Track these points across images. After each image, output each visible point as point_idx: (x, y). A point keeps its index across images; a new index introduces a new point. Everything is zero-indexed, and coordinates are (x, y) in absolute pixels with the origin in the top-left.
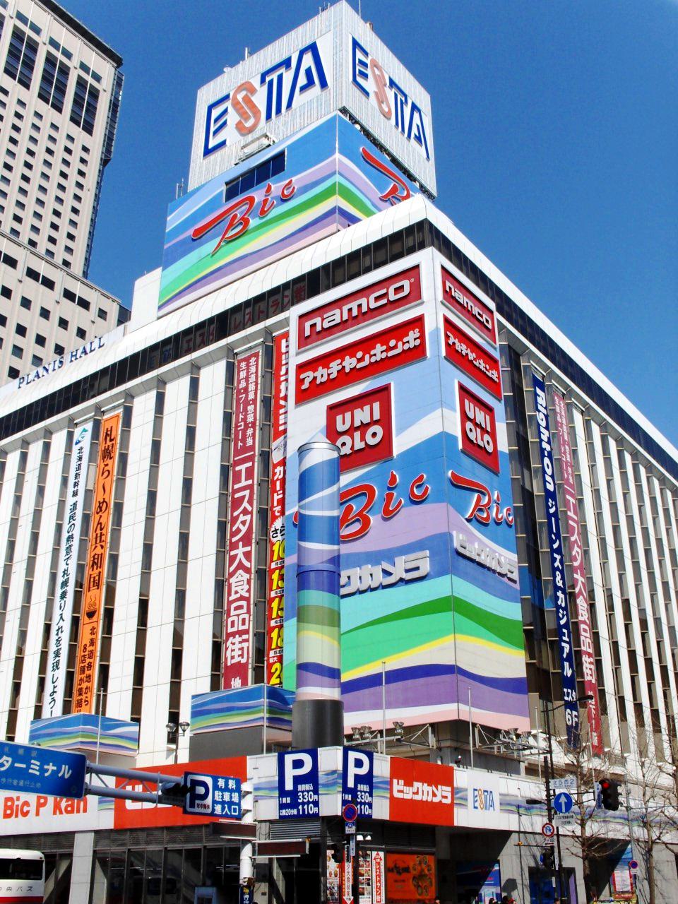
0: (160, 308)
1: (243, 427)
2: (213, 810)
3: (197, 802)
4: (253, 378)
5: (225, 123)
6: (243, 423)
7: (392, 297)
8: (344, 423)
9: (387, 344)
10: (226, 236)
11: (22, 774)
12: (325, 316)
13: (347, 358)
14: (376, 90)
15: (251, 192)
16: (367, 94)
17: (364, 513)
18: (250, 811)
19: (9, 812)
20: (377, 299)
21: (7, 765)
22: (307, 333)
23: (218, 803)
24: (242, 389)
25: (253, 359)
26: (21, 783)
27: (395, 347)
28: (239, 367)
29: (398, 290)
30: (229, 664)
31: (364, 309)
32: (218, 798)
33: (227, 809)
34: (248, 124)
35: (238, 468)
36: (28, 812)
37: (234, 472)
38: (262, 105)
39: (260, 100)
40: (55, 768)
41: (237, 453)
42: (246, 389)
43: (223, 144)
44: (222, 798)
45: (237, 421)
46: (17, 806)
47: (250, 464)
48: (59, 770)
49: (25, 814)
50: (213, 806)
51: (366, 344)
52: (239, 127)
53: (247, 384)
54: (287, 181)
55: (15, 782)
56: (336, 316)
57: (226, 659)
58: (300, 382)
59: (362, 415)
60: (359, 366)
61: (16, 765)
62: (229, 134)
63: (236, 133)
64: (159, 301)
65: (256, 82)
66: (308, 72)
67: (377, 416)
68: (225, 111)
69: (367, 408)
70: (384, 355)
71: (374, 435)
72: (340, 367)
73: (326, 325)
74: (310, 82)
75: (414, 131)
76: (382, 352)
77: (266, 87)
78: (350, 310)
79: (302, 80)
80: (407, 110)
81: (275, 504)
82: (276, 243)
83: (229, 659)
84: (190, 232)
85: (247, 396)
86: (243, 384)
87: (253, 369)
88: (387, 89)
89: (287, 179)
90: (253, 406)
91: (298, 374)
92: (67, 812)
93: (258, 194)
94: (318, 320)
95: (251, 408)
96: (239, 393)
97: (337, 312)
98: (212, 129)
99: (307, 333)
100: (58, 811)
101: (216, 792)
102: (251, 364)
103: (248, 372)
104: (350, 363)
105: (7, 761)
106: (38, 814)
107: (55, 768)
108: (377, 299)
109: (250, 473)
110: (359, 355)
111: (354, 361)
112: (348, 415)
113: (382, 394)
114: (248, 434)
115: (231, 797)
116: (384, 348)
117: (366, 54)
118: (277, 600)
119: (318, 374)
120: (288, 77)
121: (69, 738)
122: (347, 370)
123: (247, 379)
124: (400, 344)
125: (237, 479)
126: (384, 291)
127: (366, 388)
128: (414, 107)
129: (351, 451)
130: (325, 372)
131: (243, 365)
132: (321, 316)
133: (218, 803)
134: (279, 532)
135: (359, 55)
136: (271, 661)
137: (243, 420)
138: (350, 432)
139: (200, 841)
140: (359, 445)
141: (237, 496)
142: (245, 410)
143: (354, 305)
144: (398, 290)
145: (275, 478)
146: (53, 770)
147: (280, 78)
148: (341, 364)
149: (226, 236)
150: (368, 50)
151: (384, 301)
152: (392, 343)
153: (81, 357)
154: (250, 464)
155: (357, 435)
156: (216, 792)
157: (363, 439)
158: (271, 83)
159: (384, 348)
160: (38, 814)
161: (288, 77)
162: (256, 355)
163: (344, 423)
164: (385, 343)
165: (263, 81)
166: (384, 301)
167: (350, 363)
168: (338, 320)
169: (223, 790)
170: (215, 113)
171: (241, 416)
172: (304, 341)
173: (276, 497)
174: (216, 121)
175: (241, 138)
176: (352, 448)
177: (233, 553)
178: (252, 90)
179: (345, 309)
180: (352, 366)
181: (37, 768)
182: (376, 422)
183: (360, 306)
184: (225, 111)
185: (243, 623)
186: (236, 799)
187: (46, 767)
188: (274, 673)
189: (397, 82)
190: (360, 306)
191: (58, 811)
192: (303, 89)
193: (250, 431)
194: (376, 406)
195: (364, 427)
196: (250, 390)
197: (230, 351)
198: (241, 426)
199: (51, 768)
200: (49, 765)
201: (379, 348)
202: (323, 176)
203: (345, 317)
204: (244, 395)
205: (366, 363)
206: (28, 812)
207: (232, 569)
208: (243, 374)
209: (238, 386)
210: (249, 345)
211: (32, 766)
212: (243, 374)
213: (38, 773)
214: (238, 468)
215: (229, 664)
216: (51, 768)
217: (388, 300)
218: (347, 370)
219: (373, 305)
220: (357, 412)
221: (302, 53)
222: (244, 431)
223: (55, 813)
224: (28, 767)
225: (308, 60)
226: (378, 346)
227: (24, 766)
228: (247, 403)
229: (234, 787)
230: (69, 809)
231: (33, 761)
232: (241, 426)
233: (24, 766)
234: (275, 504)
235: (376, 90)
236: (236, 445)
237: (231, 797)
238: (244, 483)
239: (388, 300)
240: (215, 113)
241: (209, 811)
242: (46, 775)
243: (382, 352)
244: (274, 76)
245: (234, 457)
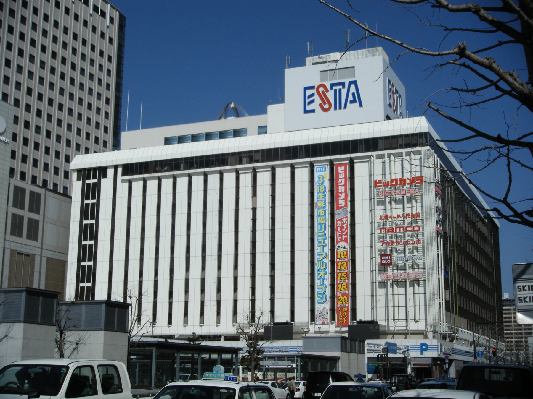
52: (321, 105)
66: (353, 94)
67: (389, 258)
79: (351, 98)
81: (338, 236)
118: (340, 273)
120: (344, 92)
134: (340, 247)
136: (338, 295)
140: (386, 262)
145: (338, 225)
155: (386, 261)
161: (344, 92)
173: (338, 233)
188: (340, 300)
194: (389, 257)
195: (387, 260)
200: (301, 362)
220: (386, 257)
225: (353, 89)
230: (424, 347)
234: (338, 236)
237: (487, 362)
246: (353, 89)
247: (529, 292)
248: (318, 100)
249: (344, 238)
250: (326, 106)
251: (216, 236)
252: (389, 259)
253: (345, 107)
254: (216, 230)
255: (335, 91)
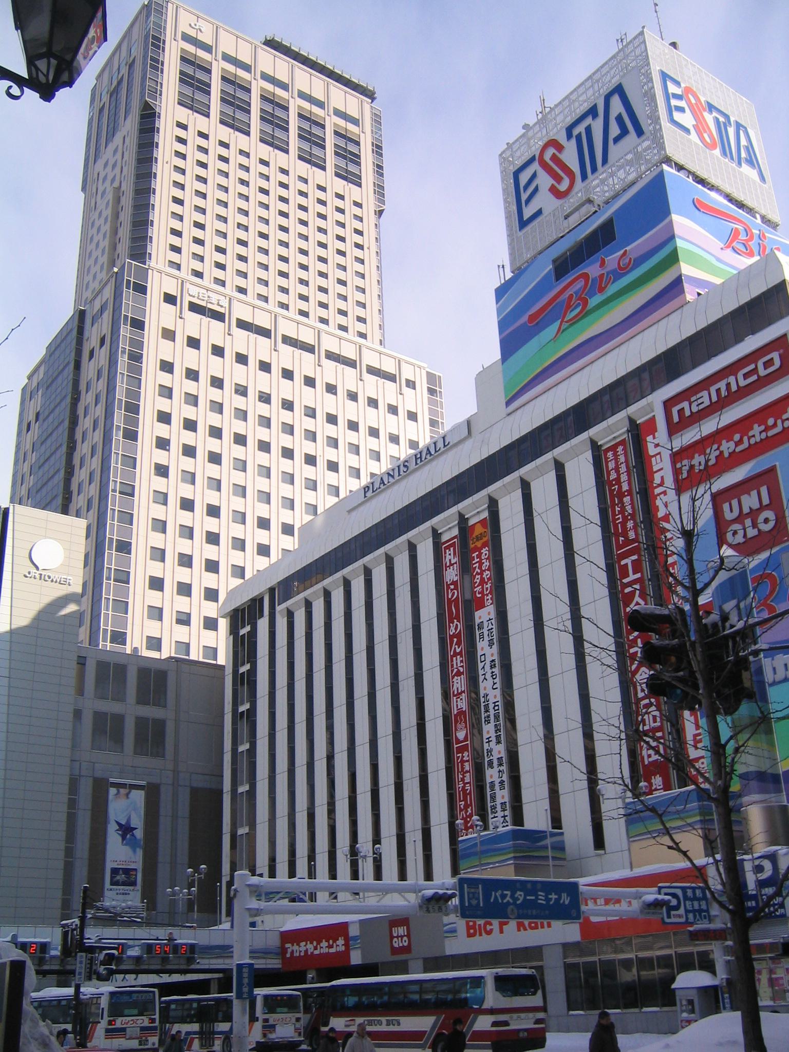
0: (508, 403)
1: (621, 520)
2: (687, 918)
3: (673, 913)
4: (623, 468)
5: (536, 189)
6: (620, 516)
7: (762, 372)
8: (731, 511)
9: (765, 423)
10: (565, 320)
11: (533, 904)
12: (693, 399)
13: (724, 442)
14: (695, 123)
15: (583, 269)
16: (687, 131)
17: (768, 602)
18: (717, 916)
19: (472, 931)
20: (746, 376)
21: (521, 898)
22: (676, 418)
23: (690, 911)
24: (613, 480)
25: (620, 448)
26: (534, 912)
27: (775, 425)
28: (606, 458)
29: (767, 364)
30: (646, 763)
31: (734, 388)
32: (689, 907)
33: (698, 916)
34: (563, 187)
35: (623, 563)
36: (491, 930)
37: (620, 566)
38: (575, 167)
39: (570, 157)
40: (556, 897)
41: (619, 547)
42: (618, 480)
43: (539, 213)
44: (693, 907)
45: (614, 514)
46: (480, 925)
47: (635, 557)
48: (560, 898)
49: (489, 933)
50: (686, 915)
51: (742, 424)
52: (554, 190)
53: (619, 475)
54: (622, 252)
55: (529, 912)
56: (704, 398)
57: (643, 758)
58: (676, 472)
59: (750, 501)
60: (738, 450)
61: (528, 898)
62: (544, 200)
63: (551, 197)
64: (506, 398)
65: (562, 138)
66: (619, 119)
67: (766, 501)
68: (534, 176)
69: (754, 493)
70: (764, 436)
71: (766, 521)
72: (717, 453)
73: (695, 409)
74: (624, 132)
75: (743, 155)
76: (761, 433)
77: (573, 141)
78: (718, 391)
79: (615, 130)
80: (731, 131)
82: (618, 324)
83: (646, 758)
84: (525, 318)
85: (620, 487)
86: (613, 476)
87: (622, 459)
88: (706, 115)
89: (620, 250)
90: (629, 497)
91: (674, 463)
92: (532, 928)
93: (593, 270)
94: (685, 405)
95: (627, 500)
96: (611, 485)
97: (705, 394)
98: (524, 197)
99: (676, 418)
100: (522, 928)
101: (687, 902)
102: (619, 453)
103: (616, 463)
104: (727, 447)
105: (521, 895)
106: (501, 932)
107: (556, 897)
108: (746, 376)
109: (637, 566)
110: (737, 437)
111: (731, 445)
112: (735, 503)
113: (768, 476)
114: (628, 526)
115: (700, 905)
116: (763, 427)
117: (678, 83)
119: (695, 462)
120: (597, 126)
121: (505, 854)
122: (726, 455)
123: (617, 469)
124: (779, 422)
125: (624, 572)
126: (752, 366)
127: (750, 471)
128: (738, 126)
129: (744, 540)
130: (702, 459)
131: (610, 454)
132: (689, 400)
133: (690, 911)
135: (672, 89)
137: (620, 512)
138: (740, 519)
139: (669, 947)
140: (752, 532)
141: (627, 590)
142: (621, 501)
143: (722, 385)
144: (767, 364)
146: (556, 899)
147: (588, 130)
148: (718, 449)
149: (565, 320)
150: (679, 79)
151: (755, 378)
152: (771, 422)
153: (426, 458)
154: (635, 557)
156: (687, 902)
157: (754, 525)
158: (579, 137)
159: (763, 427)
160: (501, 932)
162: (622, 443)
163: (731, 511)
164: (763, 422)
165: (569, 136)
166: (755, 378)
167: (727, 447)
168: (707, 403)
169: (692, 900)
170: (524, 178)
171: (617, 509)
172: (673, 429)
174: (526, 188)
175: (561, 202)
176: (745, 536)
177: (632, 651)
178: (559, 147)
179: (713, 390)
180: (731, 450)
181: (543, 898)
182: (767, 507)
183: (728, 385)
184: (534, 176)
185: (655, 721)
186: (704, 907)
187: (550, 896)
189: (716, 105)
190: (728, 385)
191: (522, 928)
192: (617, 140)
193: (630, 524)
194: (764, 490)
195: (753, 514)
196: (622, 480)
197: (595, 446)
198: (619, 518)
199: (553, 896)
201: (757, 429)
202: (659, 243)
203: (714, 399)
204: (617, 487)
205: (745, 445)
206: (491, 930)
207: (634, 667)
208: (611, 465)
209: (608, 477)
210: (613, 436)
211: (540, 897)
212: (611, 465)
213: (544, 902)
214: (623, 563)
215: (646, 763)
216: (553, 896)
217: (758, 376)
218: (726, 455)
219: (742, 383)
220: (744, 498)
221: (607, 98)
222: (624, 524)
223: (519, 930)
224: (537, 899)
225: (617, 106)
226: (756, 426)
227: (533, 898)
228: (621, 495)
229: (701, 895)
231: (540, 893)
232: (619, 518)
233: (533, 898)
235: (695, 123)
236: (617, 541)
237: (700, 905)
238: (632, 577)
239: (758, 376)
240: (524, 178)
241: (683, 920)
242: (551, 903)
243: (761, 433)
244: (580, 129)
245: (617, 551)
246: (617, 106)
247: (459, 930)
248: (544, 181)
249: (634, 573)
250: (563, 187)
251: (535, 689)
252: (762, 508)
253: (605, 161)
254: (534, 675)
255: (579, 137)
